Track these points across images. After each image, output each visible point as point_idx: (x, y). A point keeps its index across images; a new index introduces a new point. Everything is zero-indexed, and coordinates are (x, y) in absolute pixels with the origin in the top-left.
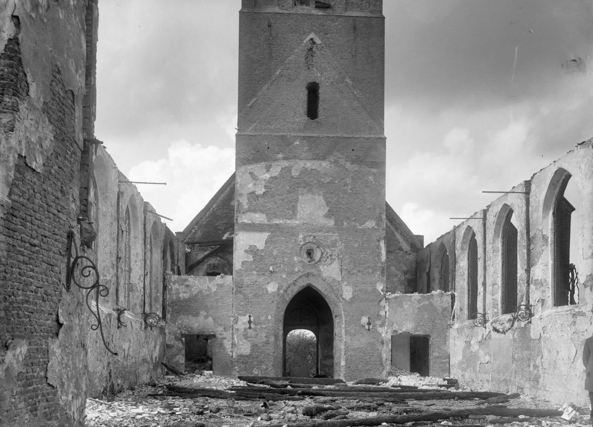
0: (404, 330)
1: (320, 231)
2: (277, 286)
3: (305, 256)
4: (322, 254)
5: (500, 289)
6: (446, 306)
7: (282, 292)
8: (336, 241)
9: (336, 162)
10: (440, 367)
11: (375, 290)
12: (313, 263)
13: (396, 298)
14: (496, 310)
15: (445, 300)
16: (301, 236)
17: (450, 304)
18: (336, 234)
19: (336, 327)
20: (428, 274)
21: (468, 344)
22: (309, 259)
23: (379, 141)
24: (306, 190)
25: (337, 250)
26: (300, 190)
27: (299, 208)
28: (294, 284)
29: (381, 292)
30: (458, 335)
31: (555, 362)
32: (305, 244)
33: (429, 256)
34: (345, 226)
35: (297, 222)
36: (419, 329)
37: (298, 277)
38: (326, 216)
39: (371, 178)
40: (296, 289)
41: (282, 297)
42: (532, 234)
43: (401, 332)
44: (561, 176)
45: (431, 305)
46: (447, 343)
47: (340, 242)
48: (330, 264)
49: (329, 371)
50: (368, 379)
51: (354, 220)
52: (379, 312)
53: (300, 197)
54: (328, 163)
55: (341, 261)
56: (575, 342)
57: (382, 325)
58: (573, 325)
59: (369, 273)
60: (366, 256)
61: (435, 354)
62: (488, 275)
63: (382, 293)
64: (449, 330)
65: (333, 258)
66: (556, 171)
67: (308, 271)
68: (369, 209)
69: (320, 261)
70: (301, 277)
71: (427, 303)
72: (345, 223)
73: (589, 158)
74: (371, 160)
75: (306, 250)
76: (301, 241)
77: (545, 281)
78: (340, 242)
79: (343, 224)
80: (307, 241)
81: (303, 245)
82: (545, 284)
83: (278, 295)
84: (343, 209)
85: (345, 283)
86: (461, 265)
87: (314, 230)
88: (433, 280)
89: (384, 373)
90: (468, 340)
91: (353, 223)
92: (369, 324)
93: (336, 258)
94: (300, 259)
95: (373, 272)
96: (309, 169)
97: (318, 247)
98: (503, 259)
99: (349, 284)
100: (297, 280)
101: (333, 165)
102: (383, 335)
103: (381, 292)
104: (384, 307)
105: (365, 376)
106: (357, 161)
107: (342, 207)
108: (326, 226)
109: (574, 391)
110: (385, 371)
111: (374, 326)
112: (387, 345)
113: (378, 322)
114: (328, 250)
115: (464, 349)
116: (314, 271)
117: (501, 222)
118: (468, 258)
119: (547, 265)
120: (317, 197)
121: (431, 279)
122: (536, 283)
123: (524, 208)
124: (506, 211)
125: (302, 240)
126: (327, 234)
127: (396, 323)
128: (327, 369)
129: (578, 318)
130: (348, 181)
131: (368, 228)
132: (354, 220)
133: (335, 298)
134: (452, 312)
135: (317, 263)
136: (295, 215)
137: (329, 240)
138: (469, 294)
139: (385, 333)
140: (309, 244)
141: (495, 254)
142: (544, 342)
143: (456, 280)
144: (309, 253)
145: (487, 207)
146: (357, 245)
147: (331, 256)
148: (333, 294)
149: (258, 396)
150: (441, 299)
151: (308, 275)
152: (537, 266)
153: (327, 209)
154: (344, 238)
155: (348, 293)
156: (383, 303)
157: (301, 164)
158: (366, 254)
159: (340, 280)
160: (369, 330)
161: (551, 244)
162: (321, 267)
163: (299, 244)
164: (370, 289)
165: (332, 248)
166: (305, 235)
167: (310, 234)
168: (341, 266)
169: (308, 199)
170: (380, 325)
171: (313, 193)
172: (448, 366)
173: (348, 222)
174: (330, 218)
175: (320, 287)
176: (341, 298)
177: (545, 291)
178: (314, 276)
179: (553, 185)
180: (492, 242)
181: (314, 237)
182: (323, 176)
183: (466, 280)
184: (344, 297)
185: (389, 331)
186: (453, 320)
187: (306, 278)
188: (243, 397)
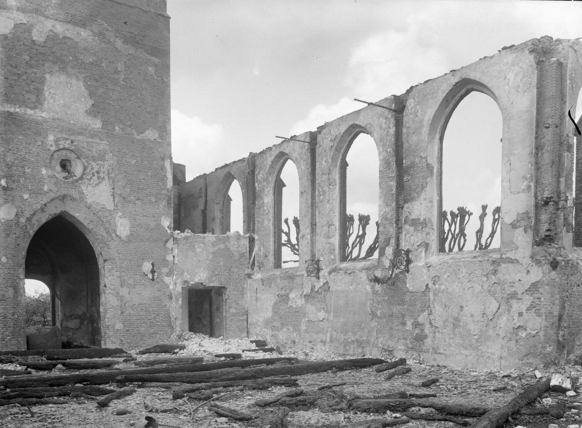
0: (197, 280)
1: (81, 134)
2: (14, 211)
3: (59, 168)
4: (85, 168)
5: (338, 231)
6: (243, 252)
7: (23, 220)
8: (105, 152)
9: (101, 34)
10: (237, 326)
11: (159, 226)
12: (71, 180)
13: (186, 238)
14: (332, 257)
15: (242, 243)
16: (51, 138)
17: (248, 250)
18: (104, 142)
19: (107, 275)
20: (204, 213)
21: (284, 298)
22: (66, 174)
23: (161, 19)
24: (56, 68)
25: (106, 166)
26: (47, 65)
27: (47, 94)
28: (42, 210)
29: (167, 229)
30: (263, 287)
31: (457, 319)
32: (58, 150)
33: (204, 189)
34: (117, 131)
35: (44, 115)
36: (214, 279)
37: (49, 200)
38: (88, 113)
39: (151, 69)
40: (44, 218)
41: (24, 228)
42: (406, 162)
43: (193, 283)
44: (461, 89)
45: (227, 249)
46: (245, 296)
47: (111, 154)
48: (97, 185)
49: (75, 336)
50: (158, 346)
51: (130, 126)
52: (165, 256)
53: (47, 76)
54: (91, 34)
55: (113, 181)
56: (497, 295)
57: (170, 274)
58: (493, 275)
59: (151, 202)
60: (146, 178)
61: (232, 310)
62: (319, 213)
63: (169, 231)
64: (247, 281)
65: (102, 176)
66: (457, 83)
67: (64, 192)
68: (150, 113)
69: (81, 178)
70: (53, 200)
71: (222, 246)
72: (117, 128)
73: (524, 66)
74: (150, 44)
75: (59, 161)
76: (51, 146)
77: (430, 221)
78: (111, 154)
79: (113, 128)
80: (61, 147)
81: (56, 151)
82: (429, 225)
83: (17, 224)
84: (114, 106)
85: (120, 214)
86: (266, 201)
87: (71, 131)
88: (213, 219)
89: (174, 337)
90: (283, 292)
91: (129, 130)
92: (153, 272)
93: (105, 176)
94: (50, 172)
95: (156, 201)
96: (61, 37)
97: (78, 158)
98: (341, 194)
99: (124, 216)
100: (48, 205)
101: (97, 38)
102: (171, 287)
103: (167, 229)
104: (172, 250)
105: (151, 343)
106: (133, 40)
107: (112, 103)
108: (90, 128)
109: (493, 354)
110: (174, 334)
111: (160, 274)
112: (177, 300)
113: (165, 270)
114: (94, 164)
115: (276, 303)
116: (74, 193)
117: (341, 148)
118: (274, 194)
119: (431, 202)
120: (74, 81)
121: (209, 219)
122: (415, 223)
123: (392, 130)
124: (350, 134)
125: (52, 143)
126: (91, 140)
127: (188, 271)
128: (70, 334)
129: (503, 265)
130: (120, 67)
131: (149, 140)
132: (130, 126)
133: (104, 234)
134: (250, 258)
135: (77, 181)
136: (41, 104)
137: (94, 150)
138: (275, 237)
139: (175, 285)
140: (64, 152)
141: (331, 187)
142: (435, 294)
143: (256, 219)
144: (64, 165)
145: (318, 128)
146: (135, 161)
147: (98, 172)
148: (102, 229)
149: (56, 393)
150: (238, 242)
151: (63, 198)
152: (417, 203)
153: (91, 102)
154: (116, 149)
155: (123, 228)
156: (170, 244)
157: (49, 24)
158: (147, 176)
159: (112, 207)
160: (153, 279)
161: (437, 176)
162: (83, 188)
163: (49, 150)
164: (153, 224)
165: (100, 162)
166: (58, 136)
167: (65, 136)
168: (113, 189)
169: (61, 82)
170: (167, 273)
171: (68, 75)
172: (246, 325)
173: (121, 126)
174: (95, 116)
175: (79, 215)
176: (114, 235)
177: (429, 234)
178: (73, 199)
179: (447, 101)
180: (326, 172)
181: (72, 142)
182: (82, 51)
183: (272, 220)
184: (118, 234)
185: (179, 281)
186: (252, 268)
187: (60, 202)
188: (34, 399)
